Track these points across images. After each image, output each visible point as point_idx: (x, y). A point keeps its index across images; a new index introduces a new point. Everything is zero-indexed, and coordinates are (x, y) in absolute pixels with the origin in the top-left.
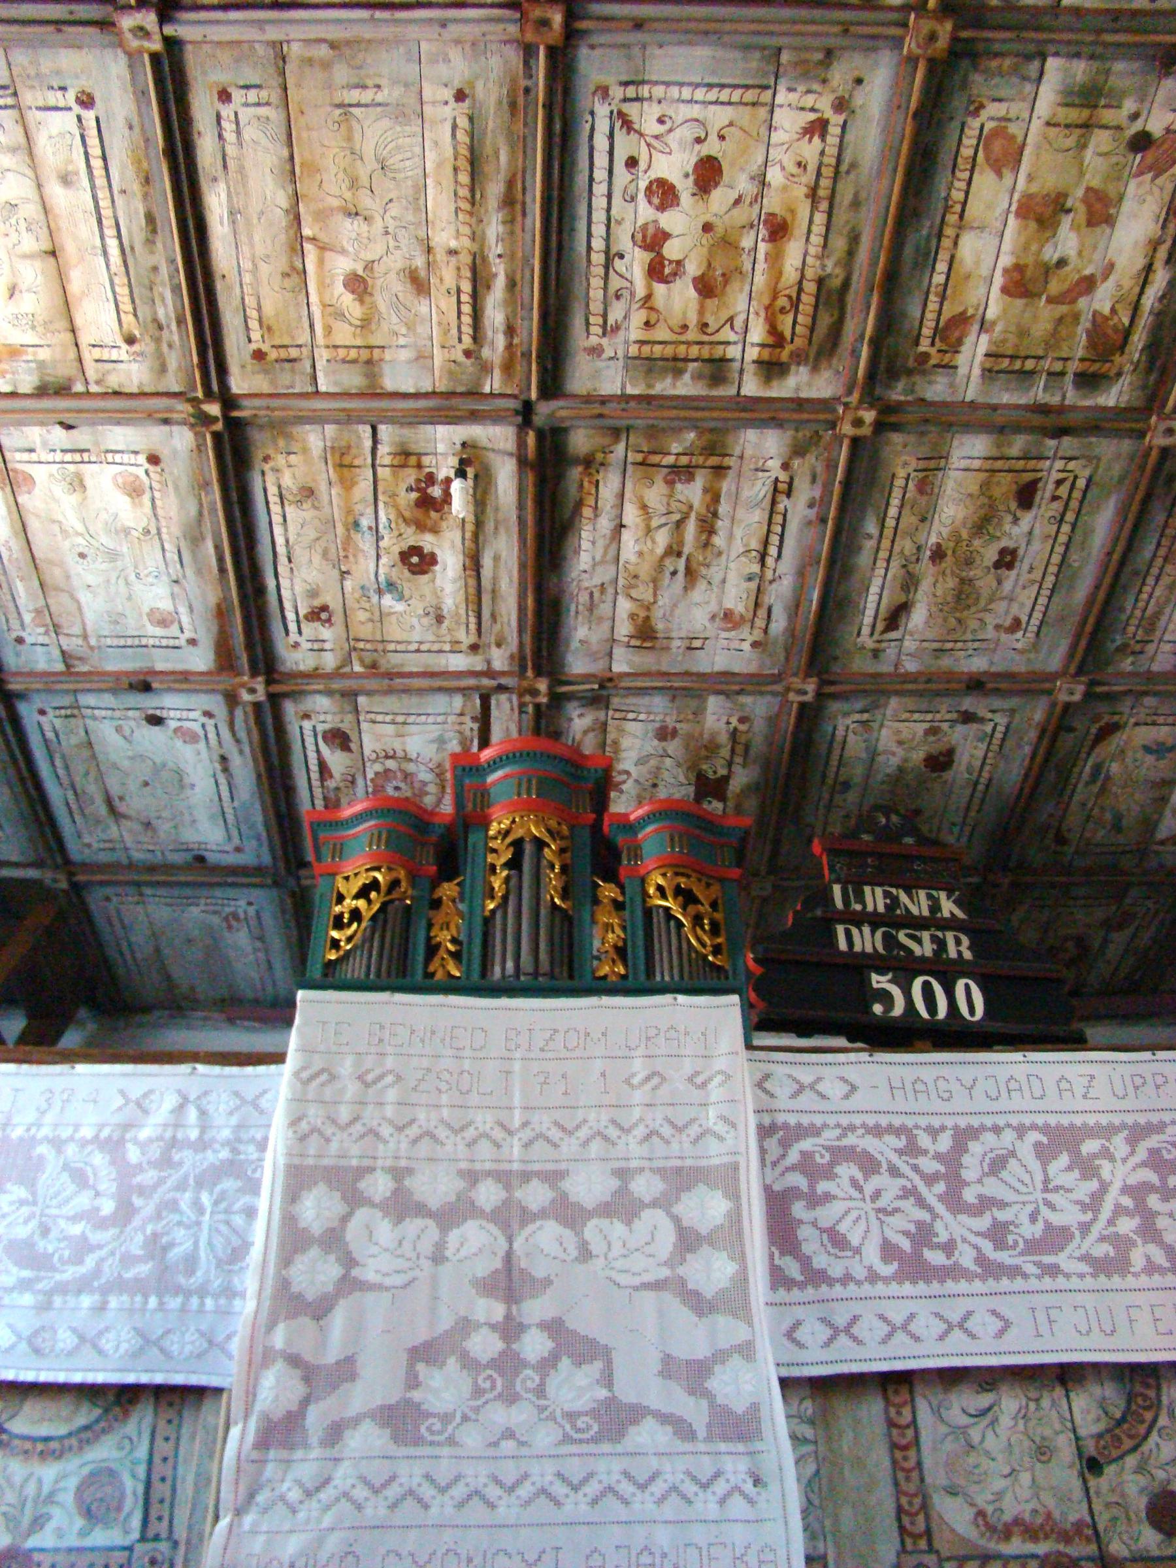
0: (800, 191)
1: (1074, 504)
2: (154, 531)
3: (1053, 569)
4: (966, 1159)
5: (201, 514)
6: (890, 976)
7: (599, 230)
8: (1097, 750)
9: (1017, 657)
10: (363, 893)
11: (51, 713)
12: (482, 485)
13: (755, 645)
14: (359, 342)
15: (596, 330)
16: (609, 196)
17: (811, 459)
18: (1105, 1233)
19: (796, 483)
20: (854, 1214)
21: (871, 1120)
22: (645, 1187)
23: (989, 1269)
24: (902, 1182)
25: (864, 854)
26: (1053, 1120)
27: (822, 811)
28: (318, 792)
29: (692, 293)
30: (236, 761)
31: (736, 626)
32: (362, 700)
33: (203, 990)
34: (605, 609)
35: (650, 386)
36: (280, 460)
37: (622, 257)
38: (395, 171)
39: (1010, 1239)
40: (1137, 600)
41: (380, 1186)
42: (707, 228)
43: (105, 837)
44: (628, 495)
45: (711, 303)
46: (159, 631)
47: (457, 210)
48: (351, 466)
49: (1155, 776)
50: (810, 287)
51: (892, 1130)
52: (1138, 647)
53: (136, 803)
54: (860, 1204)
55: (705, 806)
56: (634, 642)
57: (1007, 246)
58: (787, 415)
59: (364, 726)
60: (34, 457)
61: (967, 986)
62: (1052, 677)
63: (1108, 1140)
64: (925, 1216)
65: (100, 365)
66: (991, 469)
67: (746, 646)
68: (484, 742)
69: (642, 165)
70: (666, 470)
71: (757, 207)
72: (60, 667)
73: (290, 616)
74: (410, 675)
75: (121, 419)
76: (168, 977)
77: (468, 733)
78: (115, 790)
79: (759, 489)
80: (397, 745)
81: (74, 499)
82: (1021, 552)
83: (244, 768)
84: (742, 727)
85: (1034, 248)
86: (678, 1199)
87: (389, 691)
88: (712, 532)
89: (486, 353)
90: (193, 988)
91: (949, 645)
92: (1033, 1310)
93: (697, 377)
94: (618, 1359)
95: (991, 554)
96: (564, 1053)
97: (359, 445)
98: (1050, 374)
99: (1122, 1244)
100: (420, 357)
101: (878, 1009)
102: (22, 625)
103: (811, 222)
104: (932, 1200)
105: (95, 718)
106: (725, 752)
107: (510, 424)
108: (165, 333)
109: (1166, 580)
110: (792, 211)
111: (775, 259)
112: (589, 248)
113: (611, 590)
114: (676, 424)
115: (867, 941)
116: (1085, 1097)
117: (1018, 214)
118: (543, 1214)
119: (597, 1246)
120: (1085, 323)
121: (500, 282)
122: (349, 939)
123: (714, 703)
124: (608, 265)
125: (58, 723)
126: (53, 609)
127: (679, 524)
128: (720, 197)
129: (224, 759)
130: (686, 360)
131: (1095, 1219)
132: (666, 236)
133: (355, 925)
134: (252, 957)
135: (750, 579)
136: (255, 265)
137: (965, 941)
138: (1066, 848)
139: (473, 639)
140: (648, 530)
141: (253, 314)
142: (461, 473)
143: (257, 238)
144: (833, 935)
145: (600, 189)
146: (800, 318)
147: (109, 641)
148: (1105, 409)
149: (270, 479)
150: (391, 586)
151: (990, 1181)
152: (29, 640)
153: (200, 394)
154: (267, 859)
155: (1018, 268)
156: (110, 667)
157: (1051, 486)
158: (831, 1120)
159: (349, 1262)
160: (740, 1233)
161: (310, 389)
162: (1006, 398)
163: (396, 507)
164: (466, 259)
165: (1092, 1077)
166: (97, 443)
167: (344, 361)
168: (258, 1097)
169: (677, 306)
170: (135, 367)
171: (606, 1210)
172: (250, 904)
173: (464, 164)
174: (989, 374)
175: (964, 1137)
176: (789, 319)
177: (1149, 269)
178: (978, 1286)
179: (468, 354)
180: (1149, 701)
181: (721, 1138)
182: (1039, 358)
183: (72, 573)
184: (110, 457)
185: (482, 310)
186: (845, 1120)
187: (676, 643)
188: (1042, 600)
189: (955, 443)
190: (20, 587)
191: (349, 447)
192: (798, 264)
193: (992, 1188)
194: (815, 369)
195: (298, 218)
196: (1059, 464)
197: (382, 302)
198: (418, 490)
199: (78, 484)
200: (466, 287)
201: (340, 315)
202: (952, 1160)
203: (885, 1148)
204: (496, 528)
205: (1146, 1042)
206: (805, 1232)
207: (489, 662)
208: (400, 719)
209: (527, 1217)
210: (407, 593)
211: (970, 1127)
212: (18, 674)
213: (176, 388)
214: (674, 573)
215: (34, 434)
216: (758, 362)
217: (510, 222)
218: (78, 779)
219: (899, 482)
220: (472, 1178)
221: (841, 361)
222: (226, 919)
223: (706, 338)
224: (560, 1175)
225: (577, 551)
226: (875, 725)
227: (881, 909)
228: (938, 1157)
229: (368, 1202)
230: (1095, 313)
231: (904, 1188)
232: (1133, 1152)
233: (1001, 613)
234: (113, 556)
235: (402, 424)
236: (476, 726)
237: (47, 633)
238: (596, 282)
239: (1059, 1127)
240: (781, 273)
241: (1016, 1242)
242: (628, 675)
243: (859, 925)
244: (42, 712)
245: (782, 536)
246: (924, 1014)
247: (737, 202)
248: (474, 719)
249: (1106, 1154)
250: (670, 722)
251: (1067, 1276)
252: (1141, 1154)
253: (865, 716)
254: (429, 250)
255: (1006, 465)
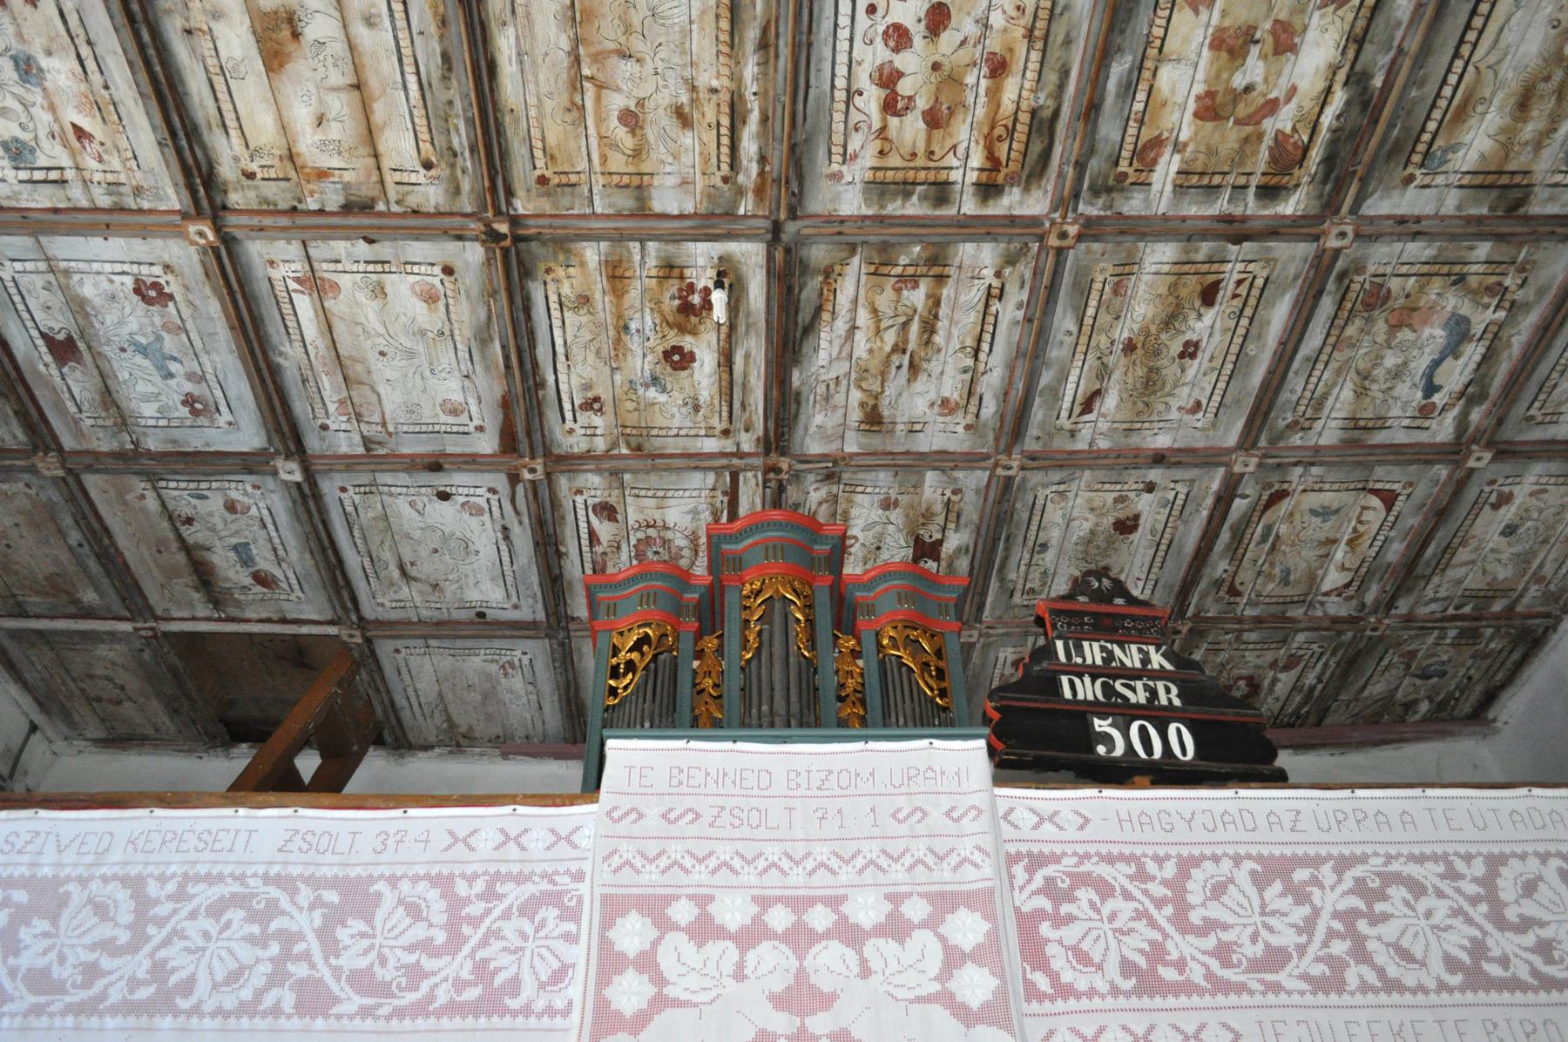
0: (1019, 32)
1: (1252, 301)
2: (447, 333)
3: (1232, 358)
4: (1190, 885)
5: (489, 318)
6: (1110, 720)
7: (842, 70)
8: (1268, 513)
9: (1198, 434)
10: (637, 647)
11: (351, 491)
12: (735, 294)
13: (968, 427)
14: (631, 169)
15: (837, 158)
16: (851, 40)
17: (1021, 267)
18: (1321, 953)
19: (1007, 288)
20: (1094, 934)
21: (1104, 849)
22: (916, 910)
23: (1221, 986)
24: (1135, 905)
25: (1082, 614)
26: (1265, 851)
27: (1023, 568)
28: (587, 557)
29: (921, 125)
30: (516, 530)
31: (952, 412)
32: (627, 477)
33: (480, 729)
34: (839, 398)
35: (882, 207)
36: (560, 272)
37: (861, 94)
38: (663, 18)
39: (1235, 957)
40: (1307, 383)
41: (683, 912)
42: (936, 67)
43: (396, 597)
44: (861, 300)
45: (938, 134)
46: (451, 420)
47: (719, 52)
48: (622, 277)
49: (1322, 536)
50: (1024, 117)
51: (1122, 858)
52: (1307, 424)
53: (426, 568)
54: (1098, 924)
55: (922, 564)
56: (863, 427)
57: (1200, 76)
58: (1001, 230)
59: (629, 500)
60: (340, 267)
61: (1179, 731)
62: (1230, 451)
63: (1317, 868)
64: (1158, 936)
65: (400, 188)
66: (1179, 271)
67: (960, 429)
68: (733, 515)
69: (880, 11)
70: (893, 280)
71: (980, 47)
72: (361, 450)
73: (567, 406)
74: (672, 456)
75: (419, 234)
76: (449, 719)
77: (718, 505)
78: (407, 559)
79: (975, 294)
80: (657, 515)
81: (376, 304)
82: (1203, 344)
83: (523, 538)
84: (954, 498)
85: (1225, 76)
86: (943, 921)
87: (654, 469)
88: (932, 331)
89: (741, 178)
90: (471, 728)
91: (1138, 425)
92: (1260, 1023)
93: (924, 198)
94: (955, 1025)
95: (1176, 347)
96: (838, 792)
97: (630, 260)
98: (1234, 187)
99: (1337, 965)
100: (684, 183)
101: (1101, 749)
102: (327, 413)
103: (1027, 61)
104: (1163, 922)
105: (391, 495)
106: (940, 519)
107: (762, 241)
108: (460, 160)
109: (1333, 365)
110: (1011, 50)
111: (994, 94)
112: (833, 86)
113: (844, 382)
114: (905, 239)
115: (1088, 690)
116: (1293, 830)
117: (1212, 46)
118: (827, 935)
119: (875, 964)
120: (1268, 141)
121: (754, 117)
122: (626, 688)
123: (931, 477)
124: (848, 101)
125: (357, 498)
126: (355, 400)
127: (905, 326)
128: (948, 39)
129: (505, 528)
130: (914, 184)
131: (1309, 942)
132: (900, 75)
133: (630, 676)
134: (524, 700)
135: (965, 372)
136: (539, 100)
137: (1174, 690)
138: (1238, 599)
139: (724, 425)
140: (878, 331)
141: (539, 144)
142: (719, 284)
143: (541, 77)
144: (1059, 686)
145: (844, 34)
146: (1015, 145)
147: (405, 428)
148: (1284, 217)
149: (552, 287)
150: (655, 380)
151: (1213, 904)
152: (333, 427)
153: (490, 214)
154: (541, 616)
155: (1210, 94)
156: (405, 451)
157: (1231, 286)
158: (1069, 849)
159: (659, 980)
160: (999, 952)
161: (589, 211)
162: (1193, 211)
163: (661, 312)
164: (725, 97)
165: (1298, 812)
166: (397, 256)
167: (617, 186)
168: (571, 834)
169: (908, 136)
170: (432, 189)
171: (880, 931)
172: (524, 653)
173: (725, 13)
174: (1179, 189)
175: (1187, 865)
176: (1005, 146)
177: (1328, 91)
178: (1208, 1000)
179: (725, 180)
180: (1315, 470)
181: (976, 865)
182: (1225, 174)
183: (373, 368)
184: (409, 267)
185: (740, 140)
186: (1081, 849)
187: (900, 427)
188: (1221, 385)
189: (1148, 250)
190: (326, 382)
191: (620, 261)
192: (1015, 98)
193: (1215, 911)
194: (1027, 189)
195: (577, 61)
196: (1240, 267)
197: (651, 134)
198: (680, 298)
199: (380, 291)
200: (725, 121)
201: (615, 146)
202: (1178, 885)
203: (1118, 875)
204: (747, 331)
205: (1345, 780)
206: (1052, 949)
207: (738, 445)
208: (660, 494)
209: (814, 937)
210: (669, 386)
211: (1192, 856)
212: (321, 457)
213: (469, 209)
214: (899, 367)
215: (340, 247)
216: (977, 184)
217: (763, 63)
218: (373, 548)
219: (1097, 286)
220: (764, 903)
221: (1050, 182)
222: (503, 667)
223: (932, 164)
224: (842, 899)
225: (816, 350)
226: (1071, 495)
227: (1099, 662)
228: (1165, 882)
229: (676, 927)
230: (1278, 132)
231: (1136, 910)
232: (1340, 881)
233: (1184, 397)
234: (410, 354)
235: (667, 242)
236: (726, 499)
237: (349, 420)
238: (838, 117)
239: (1272, 856)
240: (999, 106)
241: (1240, 962)
242: (858, 454)
243: (1080, 676)
244: (343, 490)
245: (993, 334)
246: (1143, 755)
247: (963, 43)
248: (725, 493)
249: (1316, 881)
250: (893, 494)
251: (1289, 993)
252: (1348, 883)
253: (1062, 487)
254: (694, 89)
255: (1193, 268)
